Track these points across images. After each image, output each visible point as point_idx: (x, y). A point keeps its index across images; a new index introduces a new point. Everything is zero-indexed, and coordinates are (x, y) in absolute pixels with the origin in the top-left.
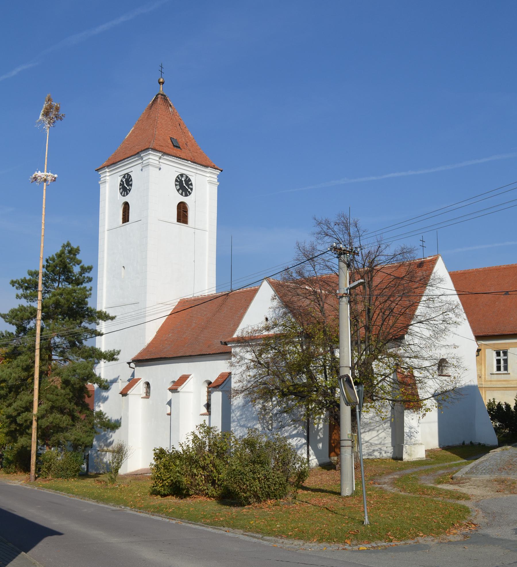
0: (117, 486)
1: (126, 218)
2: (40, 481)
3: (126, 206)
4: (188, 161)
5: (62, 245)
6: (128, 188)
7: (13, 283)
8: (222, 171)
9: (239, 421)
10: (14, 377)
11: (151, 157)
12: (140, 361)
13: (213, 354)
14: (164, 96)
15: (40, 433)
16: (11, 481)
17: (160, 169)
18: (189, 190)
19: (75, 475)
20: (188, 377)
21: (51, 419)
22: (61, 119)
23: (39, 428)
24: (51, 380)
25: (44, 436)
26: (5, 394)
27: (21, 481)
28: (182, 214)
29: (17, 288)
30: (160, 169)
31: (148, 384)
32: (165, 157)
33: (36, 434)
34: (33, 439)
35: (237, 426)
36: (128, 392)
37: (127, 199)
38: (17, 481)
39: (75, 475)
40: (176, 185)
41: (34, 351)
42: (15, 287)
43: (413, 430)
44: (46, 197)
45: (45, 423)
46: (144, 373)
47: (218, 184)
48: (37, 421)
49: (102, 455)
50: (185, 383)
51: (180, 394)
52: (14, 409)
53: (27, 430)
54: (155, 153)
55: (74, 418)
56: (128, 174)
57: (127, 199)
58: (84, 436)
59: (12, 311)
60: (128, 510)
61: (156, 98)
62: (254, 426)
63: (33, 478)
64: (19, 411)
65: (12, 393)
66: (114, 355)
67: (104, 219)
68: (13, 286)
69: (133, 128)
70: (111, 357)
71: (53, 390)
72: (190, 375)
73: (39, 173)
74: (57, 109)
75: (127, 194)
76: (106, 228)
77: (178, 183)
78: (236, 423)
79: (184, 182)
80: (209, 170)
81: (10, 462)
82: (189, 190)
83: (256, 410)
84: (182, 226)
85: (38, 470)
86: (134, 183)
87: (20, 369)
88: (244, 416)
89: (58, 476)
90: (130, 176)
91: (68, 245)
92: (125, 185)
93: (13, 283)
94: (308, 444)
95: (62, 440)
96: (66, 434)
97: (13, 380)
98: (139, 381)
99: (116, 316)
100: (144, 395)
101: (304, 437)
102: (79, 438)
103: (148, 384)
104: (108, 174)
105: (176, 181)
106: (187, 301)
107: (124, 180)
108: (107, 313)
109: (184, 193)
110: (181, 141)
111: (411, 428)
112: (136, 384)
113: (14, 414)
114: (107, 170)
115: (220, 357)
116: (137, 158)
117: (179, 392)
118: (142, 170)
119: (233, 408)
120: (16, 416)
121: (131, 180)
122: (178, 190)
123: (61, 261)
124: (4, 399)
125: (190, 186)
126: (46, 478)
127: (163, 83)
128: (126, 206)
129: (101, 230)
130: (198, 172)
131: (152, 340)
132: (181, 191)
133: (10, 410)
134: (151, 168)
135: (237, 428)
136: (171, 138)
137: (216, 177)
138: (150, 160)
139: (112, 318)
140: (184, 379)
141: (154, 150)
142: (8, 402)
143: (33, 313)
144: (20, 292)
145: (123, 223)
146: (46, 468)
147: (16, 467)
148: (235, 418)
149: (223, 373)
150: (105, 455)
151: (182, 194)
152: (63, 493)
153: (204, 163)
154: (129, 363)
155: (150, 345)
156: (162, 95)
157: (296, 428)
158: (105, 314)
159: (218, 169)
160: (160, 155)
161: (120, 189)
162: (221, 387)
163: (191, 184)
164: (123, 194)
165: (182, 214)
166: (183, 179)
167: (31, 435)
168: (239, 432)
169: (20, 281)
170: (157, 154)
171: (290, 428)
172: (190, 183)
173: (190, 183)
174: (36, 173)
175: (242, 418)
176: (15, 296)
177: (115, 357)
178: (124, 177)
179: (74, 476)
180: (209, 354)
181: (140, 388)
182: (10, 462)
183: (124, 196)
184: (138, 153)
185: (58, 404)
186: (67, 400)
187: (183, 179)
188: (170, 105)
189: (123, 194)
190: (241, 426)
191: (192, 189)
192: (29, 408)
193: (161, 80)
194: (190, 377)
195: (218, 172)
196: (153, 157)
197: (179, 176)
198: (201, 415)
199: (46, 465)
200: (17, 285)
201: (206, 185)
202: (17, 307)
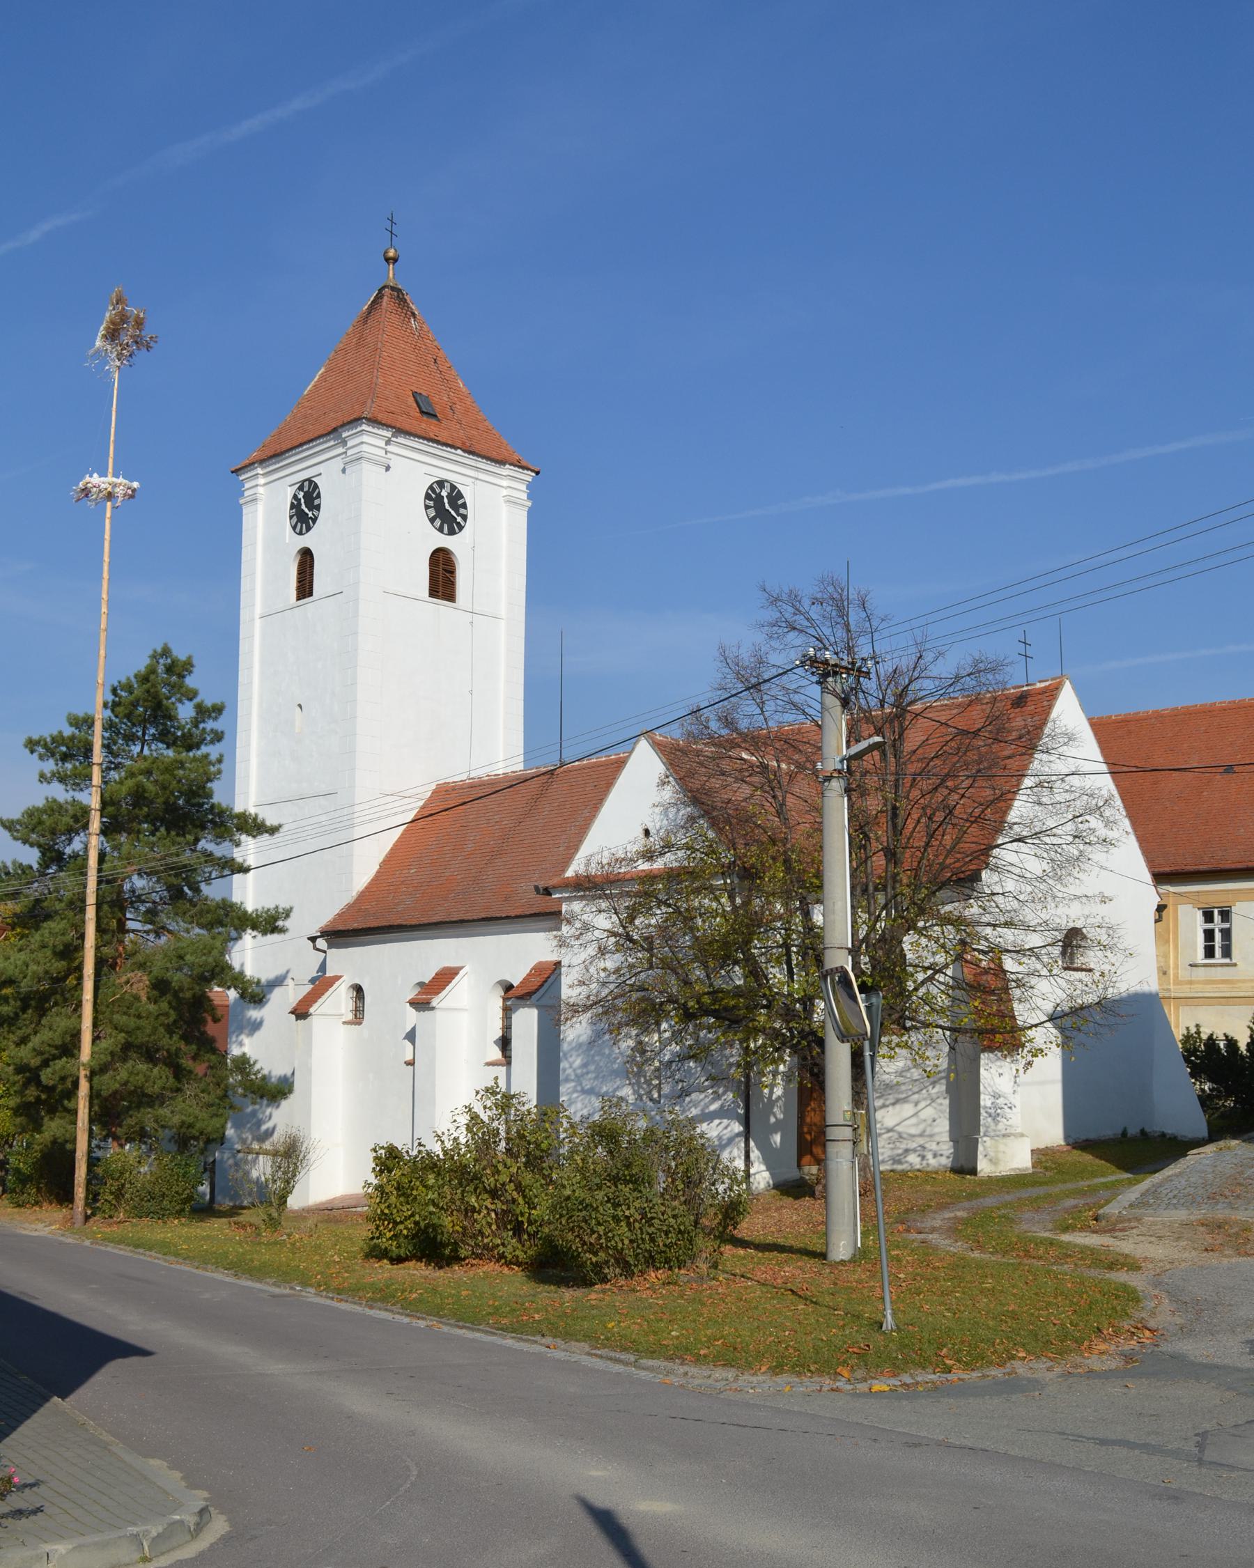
0: (285, 1237)
1: (305, 588)
2: (96, 1224)
3: (306, 558)
4: (456, 448)
5: (151, 652)
6: (310, 514)
7: (31, 745)
8: (537, 473)
9: (579, 1078)
10: (34, 973)
11: (365, 438)
12: (339, 934)
13: (517, 917)
14: (399, 291)
15: (96, 1108)
16: (27, 1225)
17: (388, 468)
18: (459, 519)
19: (183, 1210)
20: (457, 974)
21: (123, 1075)
22: (148, 348)
23: (93, 1095)
24: (124, 979)
25: (108, 1115)
26: (12, 1015)
27: (50, 1225)
28: (443, 577)
29: (41, 757)
30: (388, 468)
31: (358, 990)
32: (401, 440)
33: (87, 1111)
34: (80, 1124)
35: (575, 1091)
36: (312, 1010)
37: (308, 541)
38: (40, 1226)
39: (183, 1210)
40: (427, 507)
41: (83, 910)
42: (36, 755)
43: (1001, 1101)
44: (111, 536)
45: (109, 1083)
46: (349, 963)
47: (529, 504)
48: (90, 1080)
49: (246, 1162)
50: (448, 988)
51: (437, 1013)
52: (34, 1050)
53: (66, 1102)
54: (375, 430)
55: (179, 1073)
56: (310, 480)
57: (308, 541)
58: (204, 1115)
59: (30, 813)
60: (310, 1295)
61: (379, 297)
62: (615, 1090)
63: (80, 1217)
64: (46, 1056)
65: (30, 1011)
66: (276, 919)
67: (253, 590)
68: (32, 752)
69: (323, 370)
70: (269, 923)
71: (128, 1005)
72: (461, 968)
73: (96, 479)
74: (139, 323)
75: (309, 529)
76: (258, 610)
77: (432, 503)
78: (573, 1084)
79: (446, 500)
80: (507, 470)
81: (24, 1180)
82: (459, 519)
83: (621, 1053)
84: (442, 606)
85: (93, 1197)
86: (325, 501)
87: (49, 953)
88: (592, 1068)
89: (140, 1213)
90: (316, 486)
91: (166, 652)
92: (303, 507)
93: (31, 745)
94: (747, 1134)
95: (150, 1126)
96: (161, 1111)
97: (32, 979)
98: (338, 983)
99: (280, 826)
100: (350, 1017)
101: (737, 1117)
102: (191, 1120)
103: (358, 990)
104: (261, 481)
105: (428, 497)
106: (454, 789)
107: (301, 495)
108: (260, 817)
109: (446, 527)
110: (440, 401)
111: (996, 1096)
112: (331, 990)
113: (35, 1062)
114: (260, 471)
115: (533, 925)
116: (332, 443)
117: (433, 1008)
118: (344, 471)
119: (565, 1047)
120: (39, 1068)
121: (319, 496)
122: (432, 520)
123: (148, 691)
124: (10, 1025)
125: (462, 511)
126: (111, 1217)
127: (395, 260)
128: (306, 558)
129: (244, 615)
130: (481, 476)
131: (370, 884)
132: (438, 522)
133: (25, 1054)
134: (365, 466)
135: (575, 1095)
136: (415, 394)
137: (524, 487)
138: (365, 448)
139: (273, 830)
140: (445, 977)
141: (374, 421)
142: (19, 1033)
143: (80, 818)
144: (50, 766)
145: (299, 599)
146: (112, 1193)
147: (39, 1190)
148: (569, 1071)
149: (540, 963)
150: (255, 1161)
151: (441, 530)
152: (152, 1253)
153: (495, 455)
154: (313, 939)
155: (363, 895)
156: (393, 289)
157: (717, 1096)
158: (255, 819)
159: (528, 469)
160: (389, 434)
161: (291, 517)
162: (535, 997)
163: (464, 506)
164: (298, 530)
165: (443, 577)
166: (444, 493)
167: (75, 1112)
168: (579, 1105)
169: (49, 740)
170: (380, 432)
171: (702, 1096)
172: (460, 502)
173: (460, 502)
174: (87, 478)
175: (587, 1073)
176: (37, 777)
177: (280, 923)
178: (301, 488)
179: (179, 1213)
180: (507, 917)
181: (338, 1000)
182: (24, 1180)
183: (301, 533)
184: (335, 430)
185: (141, 1038)
186: (162, 1030)
187: (444, 493)
188: (413, 314)
189: (298, 530)
190: (584, 1092)
191: (465, 518)
192: (69, 1047)
193: (391, 253)
194: (462, 973)
195: (528, 476)
196: (370, 440)
197: (435, 486)
198: (489, 1064)
199: (112, 1185)
200: (41, 750)
201: (499, 505)
202: (40, 803)
